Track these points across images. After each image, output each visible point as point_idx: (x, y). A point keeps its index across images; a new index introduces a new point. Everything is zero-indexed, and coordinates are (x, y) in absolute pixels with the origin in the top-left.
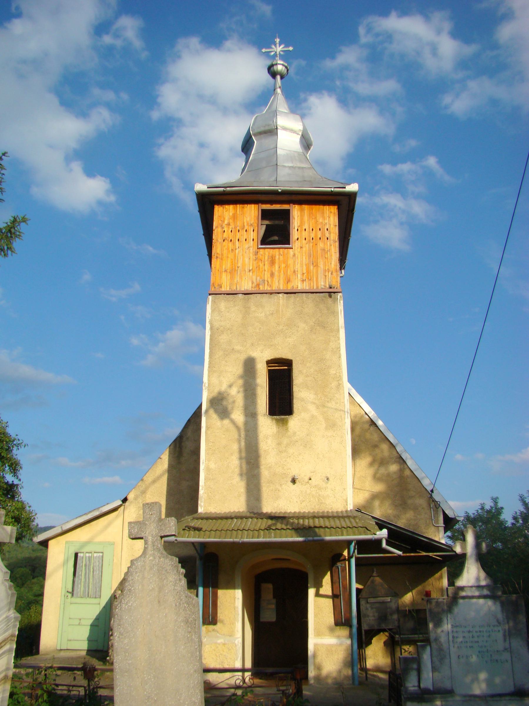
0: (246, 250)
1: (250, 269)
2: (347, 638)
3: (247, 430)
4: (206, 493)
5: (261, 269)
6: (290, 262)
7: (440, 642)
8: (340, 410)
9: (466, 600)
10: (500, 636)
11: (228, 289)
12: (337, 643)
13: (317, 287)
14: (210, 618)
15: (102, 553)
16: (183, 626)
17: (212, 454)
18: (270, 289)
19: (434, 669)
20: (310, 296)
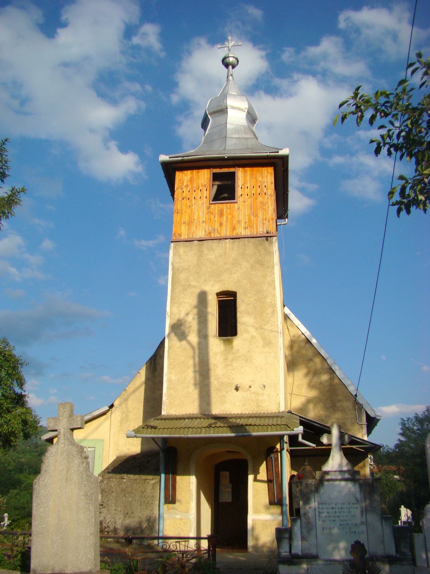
0: (201, 206)
1: (204, 221)
2: (280, 515)
3: (200, 349)
4: (167, 399)
5: (212, 221)
6: (236, 213)
7: (308, 516)
8: (274, 331)
9: (331, 482)
10: (358, 512)
11: (186, 237)
12: (271, 519)
13: (257, 233)
14: (170, 498)
15: (94, 448)
16: (83, 499)
17: (173, 368)
18: (219, 236)
19: (303, 538)
20: (251, 240)
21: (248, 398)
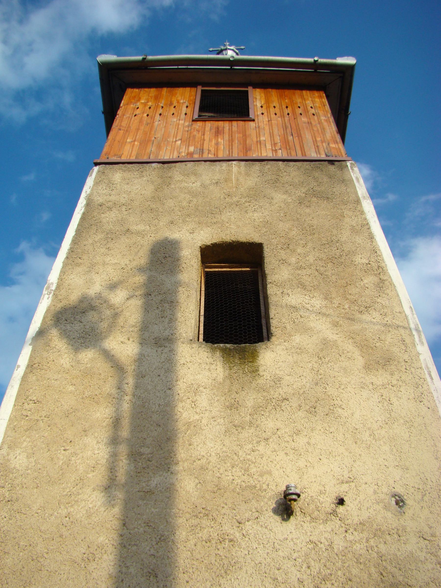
21: (335, 547)
